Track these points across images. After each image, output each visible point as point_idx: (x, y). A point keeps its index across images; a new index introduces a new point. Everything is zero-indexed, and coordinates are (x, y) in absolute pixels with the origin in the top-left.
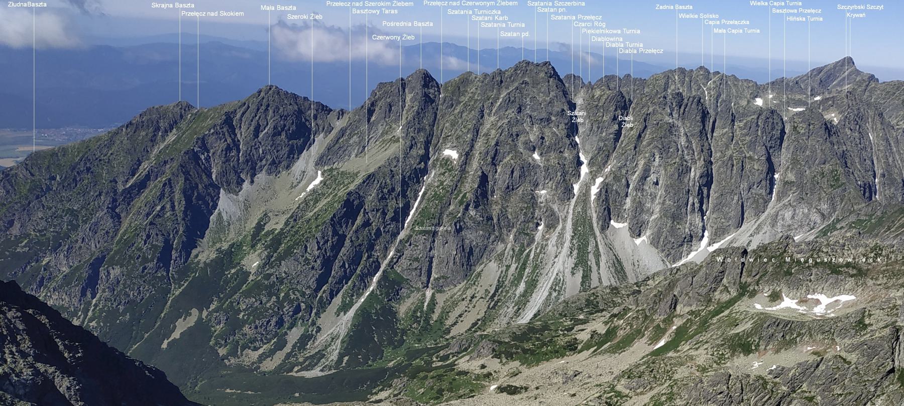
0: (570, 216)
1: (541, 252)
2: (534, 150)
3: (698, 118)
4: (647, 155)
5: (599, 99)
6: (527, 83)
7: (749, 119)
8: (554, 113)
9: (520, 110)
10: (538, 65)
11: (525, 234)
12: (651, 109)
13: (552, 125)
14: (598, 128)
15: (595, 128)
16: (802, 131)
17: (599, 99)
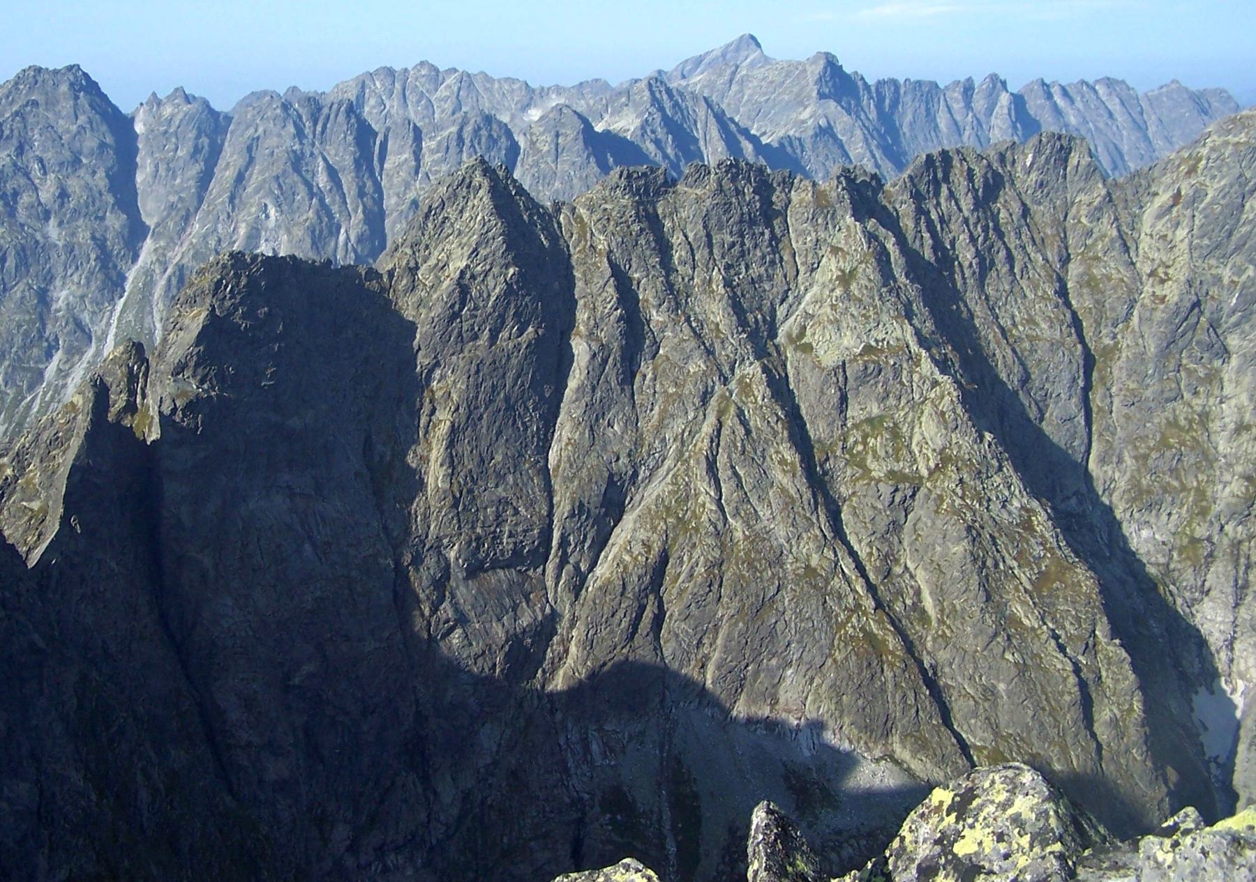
0: (113, 330)
1: (52, 398)
2: (47, 218)
3: (350, 138)
4: (253, 210)
5: (170, 121)
6: (35, 104)
7: (445, 133)
8: (85, 150)
9: (20, 150)
10: (56, 72)
11: (24, 369)
12: (261, 130)
13: (82, 172)
14: (168, 170)
15: (162, 172)
16: (546, 149)
17: (170, 121)
